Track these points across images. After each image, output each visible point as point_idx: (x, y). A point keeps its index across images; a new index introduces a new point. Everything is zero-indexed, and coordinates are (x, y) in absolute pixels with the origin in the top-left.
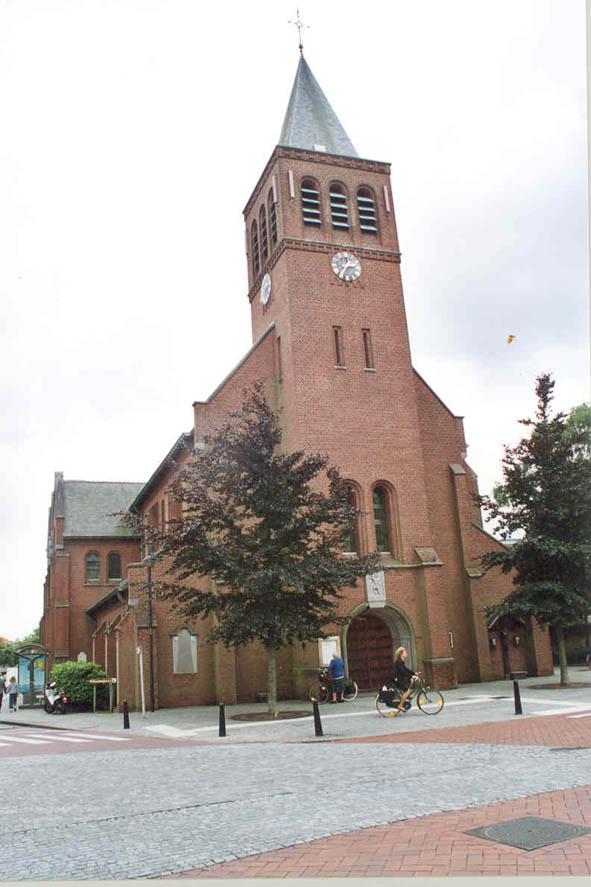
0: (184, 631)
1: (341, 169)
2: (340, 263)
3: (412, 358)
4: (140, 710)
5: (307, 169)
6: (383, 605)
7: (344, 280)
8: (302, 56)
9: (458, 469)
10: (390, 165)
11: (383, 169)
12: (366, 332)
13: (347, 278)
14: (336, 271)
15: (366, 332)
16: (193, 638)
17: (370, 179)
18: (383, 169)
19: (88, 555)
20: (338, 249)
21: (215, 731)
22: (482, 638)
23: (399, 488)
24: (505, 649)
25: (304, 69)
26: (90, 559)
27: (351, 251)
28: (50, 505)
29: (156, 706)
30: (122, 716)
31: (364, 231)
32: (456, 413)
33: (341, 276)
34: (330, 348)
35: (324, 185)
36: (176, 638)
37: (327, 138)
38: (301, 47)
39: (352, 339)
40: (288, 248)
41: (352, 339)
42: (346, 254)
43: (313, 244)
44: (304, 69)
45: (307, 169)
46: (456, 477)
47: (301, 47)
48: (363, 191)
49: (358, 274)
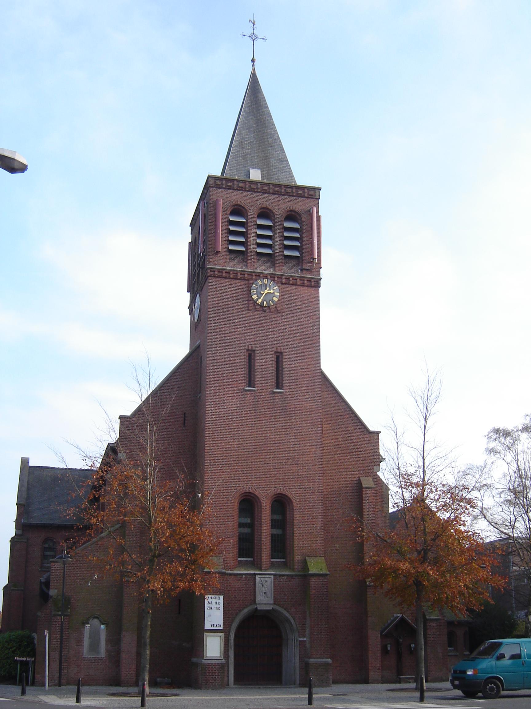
0: (96, 620)
1: (269, 196)
2: (259, 290)
3: (14, 516)
4: (44, 685)
5: (236, 197)
6: (269, 608)
7: (261, 306)
8: (254, 70)
9: (367, 482)
10: (320, 189)
11: (312, 194)
12: (279, 357)
13: (265, 304)
14: (255, 297)
15: (279, 357)
16: (103, 627)
17: (299, 205)
18: (312, 194)
19: (46, 541)
20: (259, 276)
21: (306, 698)
22: (374, 640)
23: (296, 504)
24: (399, 657)
25: (254, 88)
26: (46, 546)
27: (272, 277)
28: (77, 468)
29: (63, 681)
30: (21, 687)
31: (287, 257)
32: (372, 427)
33: (260, 301)
34: (242, 371)
35: (252, 212)
36: (88, 626)
37: (265, 166)
38: (253, 61)
39: (264, 363)
40: (210, 276)
41: (264, 363)
42: (266, 281)
43: (235, 272)
44: (254, 88)
45: (236, 197)
46: (364, 490)
47: (253, 61)
48: (292, 216)
49: (276, 299)
